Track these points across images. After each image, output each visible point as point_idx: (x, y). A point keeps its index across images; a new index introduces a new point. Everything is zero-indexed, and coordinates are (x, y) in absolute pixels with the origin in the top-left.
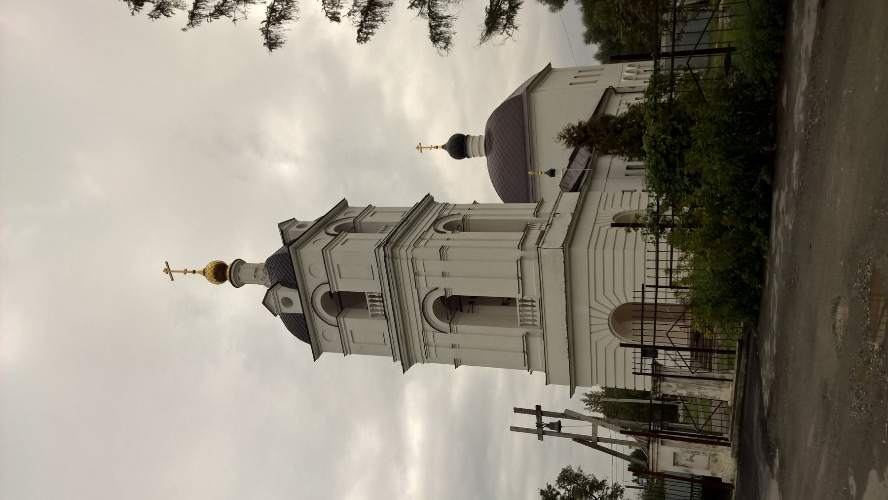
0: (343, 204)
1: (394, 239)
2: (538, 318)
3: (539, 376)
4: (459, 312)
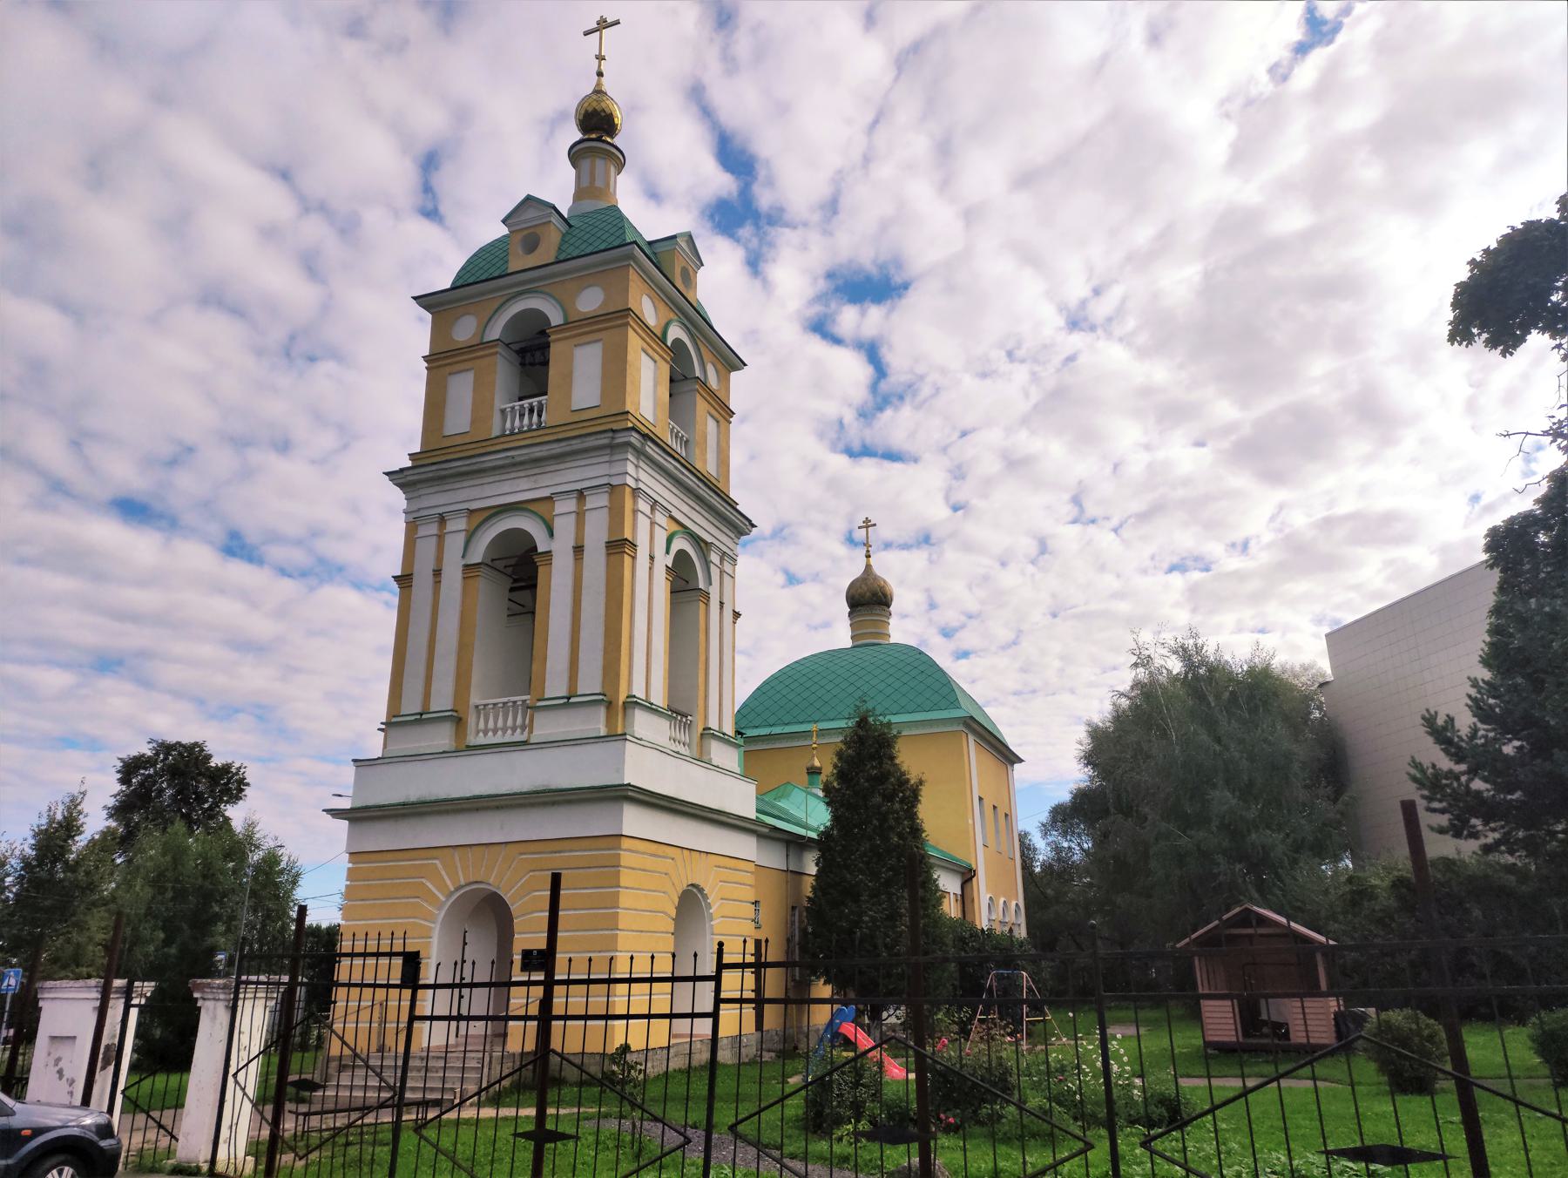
0: (731, 362)
1: (650, 449)
2: (491, 739)
3: (374, 746)
4: (508, 583)
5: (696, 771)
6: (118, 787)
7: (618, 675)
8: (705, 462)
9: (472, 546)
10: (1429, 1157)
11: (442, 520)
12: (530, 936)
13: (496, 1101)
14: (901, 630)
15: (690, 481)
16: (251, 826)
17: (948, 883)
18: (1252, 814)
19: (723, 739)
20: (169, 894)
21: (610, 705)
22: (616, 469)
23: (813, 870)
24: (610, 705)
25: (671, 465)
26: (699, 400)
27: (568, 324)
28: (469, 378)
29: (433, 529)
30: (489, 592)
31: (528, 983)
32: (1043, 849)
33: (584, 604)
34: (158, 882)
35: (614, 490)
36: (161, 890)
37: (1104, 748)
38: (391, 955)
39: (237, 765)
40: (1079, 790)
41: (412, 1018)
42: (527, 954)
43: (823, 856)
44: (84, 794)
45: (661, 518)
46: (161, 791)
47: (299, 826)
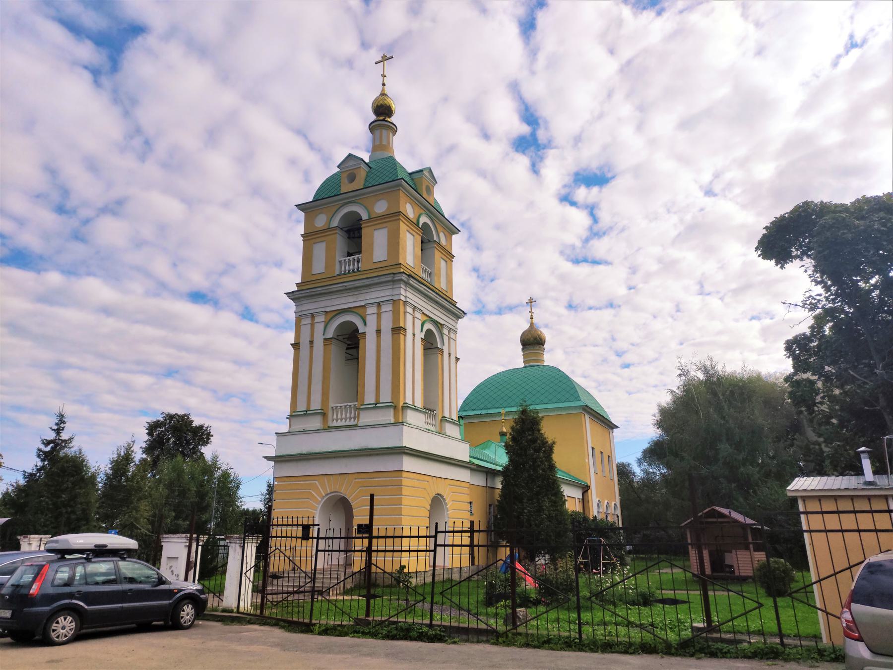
0: (452, 230)
1: (412, 281)
2: (339, 423)
3: (285, 429)
5: (438, 439)
6: (147, 438)
7: (399, 393)
8: (440, 283)
9: (327, 330)
10: (683, 602)
11: (313, 316)
12: (361, 517)
13: (346, 592)
14: (552, 357)
15: (432, 295)
16: (215, 458)
17: (568, 491)
18: (740, 457)
19: (452, 422)
20: (176, 493)
21: (395, 408)
22: (396, 292)
23: (500, 486)
24: (395, 408)
25: (422, 288)
26: (436, 252)
27: (370, 219)
28: (323, 245)
29: (308, 321)
30: (336, 351)
31: (362, 538)
32: (638, 471)
33: (382, 359)
34: (170, 486)
35: (395, 302)
36: (173, 491)
37: (668, 419)
38: (297, 525)
39: (206, 425)
40: (654, 441)
41: (317, 551)
42: (360, 526)
43: (505, 479)
44: (134, 442)
45: (418, 315)
46: (168, 439)
47: (245, 458)
